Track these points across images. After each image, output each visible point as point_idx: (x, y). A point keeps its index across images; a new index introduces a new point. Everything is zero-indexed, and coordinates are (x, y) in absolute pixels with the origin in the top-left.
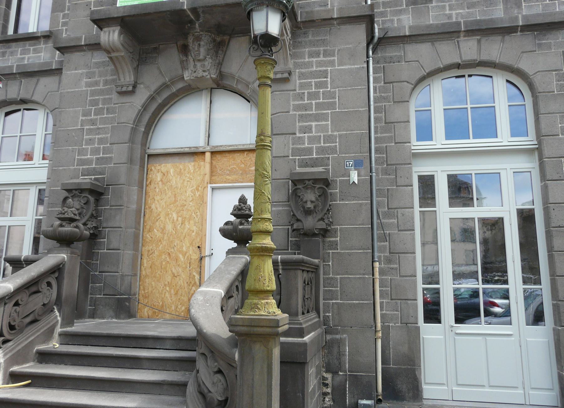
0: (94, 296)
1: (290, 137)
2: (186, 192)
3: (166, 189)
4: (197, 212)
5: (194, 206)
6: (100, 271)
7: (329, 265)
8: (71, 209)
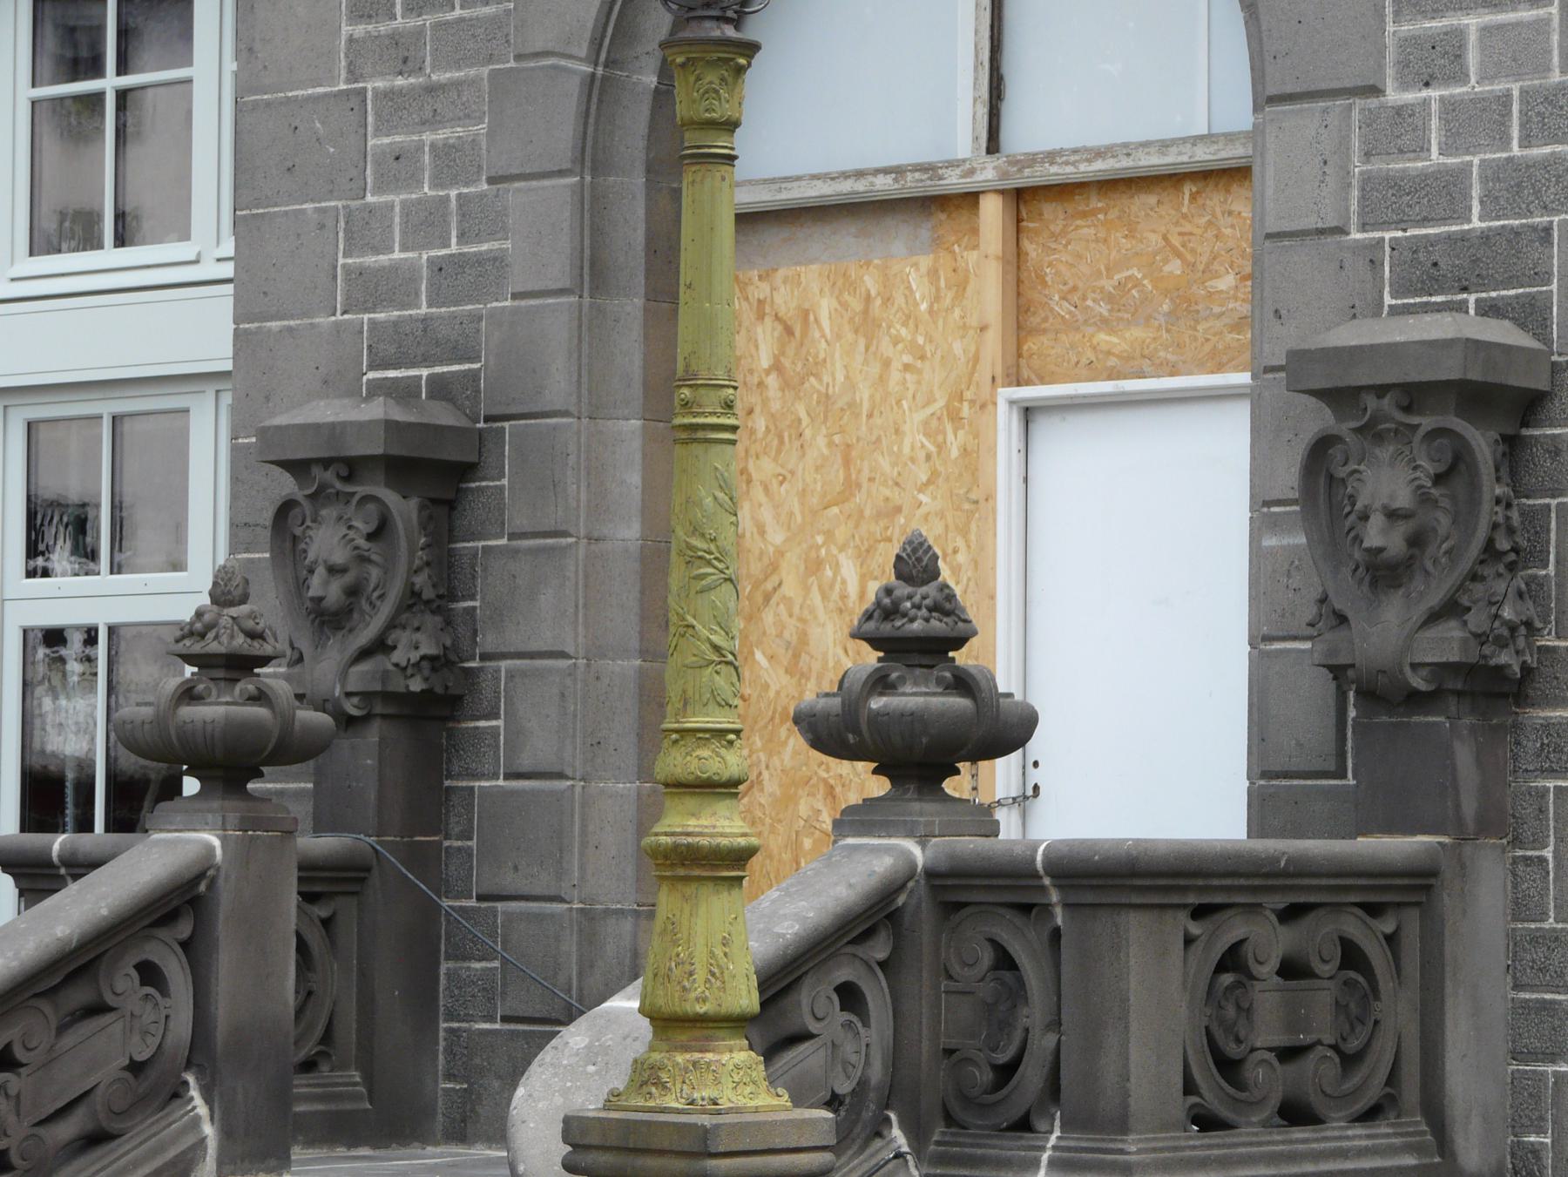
0: (464, 1025)
1: (1350, 107)
2: (897, 431)
3: (803, 414)
4: (955, 551)
5: (941, 515)
6: (485, 890)
7: (1542, 861)
8: (234, 611)
